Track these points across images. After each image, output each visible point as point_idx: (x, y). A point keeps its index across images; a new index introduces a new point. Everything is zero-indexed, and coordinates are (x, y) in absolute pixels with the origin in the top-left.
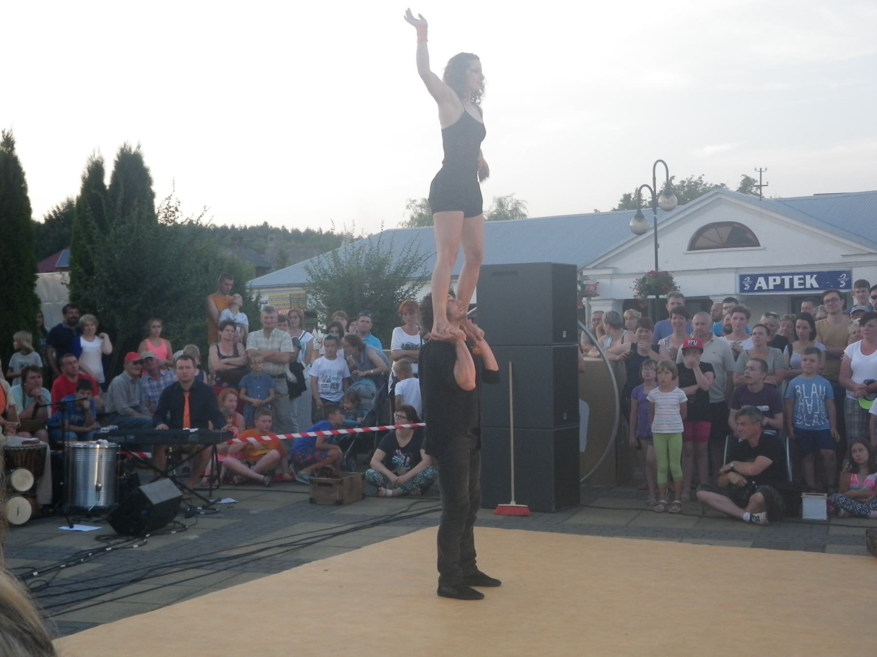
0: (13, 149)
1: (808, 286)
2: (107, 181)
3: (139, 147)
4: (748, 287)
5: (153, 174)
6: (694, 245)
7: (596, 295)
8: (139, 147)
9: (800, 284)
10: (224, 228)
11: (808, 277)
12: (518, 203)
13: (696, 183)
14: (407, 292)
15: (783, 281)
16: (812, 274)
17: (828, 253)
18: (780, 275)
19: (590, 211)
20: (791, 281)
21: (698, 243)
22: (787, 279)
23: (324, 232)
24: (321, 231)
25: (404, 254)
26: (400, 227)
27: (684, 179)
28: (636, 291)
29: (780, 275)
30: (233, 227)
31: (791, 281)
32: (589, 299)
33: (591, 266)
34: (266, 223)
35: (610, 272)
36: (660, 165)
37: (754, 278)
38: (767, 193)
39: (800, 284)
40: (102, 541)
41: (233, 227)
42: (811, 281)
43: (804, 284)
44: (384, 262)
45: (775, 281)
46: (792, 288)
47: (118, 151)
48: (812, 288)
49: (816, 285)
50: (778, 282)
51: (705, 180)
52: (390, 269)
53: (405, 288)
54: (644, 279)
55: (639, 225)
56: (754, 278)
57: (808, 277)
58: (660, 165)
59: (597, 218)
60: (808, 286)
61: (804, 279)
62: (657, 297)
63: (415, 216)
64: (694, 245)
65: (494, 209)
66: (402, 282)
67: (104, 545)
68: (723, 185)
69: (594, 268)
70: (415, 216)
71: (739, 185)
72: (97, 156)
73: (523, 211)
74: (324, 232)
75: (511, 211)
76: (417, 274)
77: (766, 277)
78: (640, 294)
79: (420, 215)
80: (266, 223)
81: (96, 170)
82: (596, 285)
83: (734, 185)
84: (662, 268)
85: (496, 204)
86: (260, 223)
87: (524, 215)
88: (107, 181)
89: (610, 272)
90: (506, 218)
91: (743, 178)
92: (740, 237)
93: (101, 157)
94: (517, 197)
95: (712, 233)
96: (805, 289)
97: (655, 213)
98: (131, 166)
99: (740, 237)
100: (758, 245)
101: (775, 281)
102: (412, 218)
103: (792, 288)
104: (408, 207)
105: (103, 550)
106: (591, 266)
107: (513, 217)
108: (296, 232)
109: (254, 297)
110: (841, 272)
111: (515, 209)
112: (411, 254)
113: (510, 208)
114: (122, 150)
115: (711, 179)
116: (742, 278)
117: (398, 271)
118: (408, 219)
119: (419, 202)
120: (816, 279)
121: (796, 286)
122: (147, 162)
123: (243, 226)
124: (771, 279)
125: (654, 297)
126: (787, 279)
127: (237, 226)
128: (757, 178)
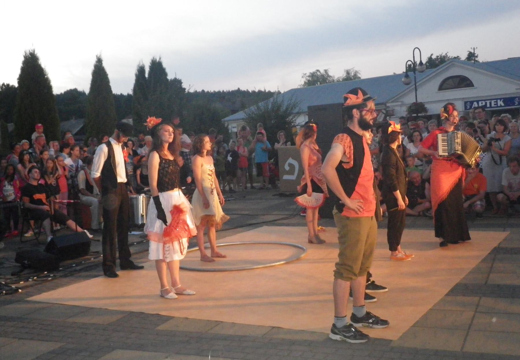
0: (102, 64)
1: (499, 105)
2: (147, 75)
3: (160, 59)
4: (468, 107)
5: (69, 89)
6: (442, 88)
7: (393, 115)
8: (160, 59)
9: (495, 104)
10: (219, 92)
11: (499, 101)
12: (356, 72)
13: (444, 57)
14: (292, 119)
15: (486, 103)
16: (500, 99)
17: (508, 88)
18: (484, 100)
19: (391, 73)
20: (490, 103)
21: (443, 87)
22: (488, 102)
23: (267, 91)
24: (265, 91)
25: (289, 102)
26: (299, 87)
27: (438, 55)
28: (406, 113)
29: (484, 100)
30: (223, 91)
31: (490, 103)
32: (390, 118)
33: (391, 101)
34: (239, 88)
35: (400, 103)
36: (417, 50)
37: (472, 103)
38: (481, 59)
39: (495, 104)
40: (143, 238)
41: (223, 91)
42: (500, 103)
43: (497, 104)
44: (279, 107)
45: (482, 103)
46: (491, 107)
47: (151, 61)
48: (501, 106)
49: (503, 105)
50: (484, 104)
51: (449, 55)
52: (284, 108)
53: (291, 117)
54: (410, 107)
55: (407, 80)
56: (472, 103)
57: (499, 101)
58: (417, 50)
59: (395, 77)
60: (499, 105)
61: (497, 102)
62: (417, 115)
63: (307, 81)
64: (442, 88)
65: (345, 75)
66: (290, 114)
67: (143, 239)
68: (458, 57)
69: (392, 102)
70: (307, 81)
71: (466, 56)
72: (141, 64)
73: (359, 75)
74: (267, 91)
75: (353, 76)
76: (296, 111)
77: (478, 102)
78: (409, 114)
79: (309, 81)
80: (239, 88)
81: (141, 70)
82: (393, 110)
83: (464, 57)
84: (419, 101)
85: (345, 73)
86: (236, 89)
87: (360, 78)
88: (147, 75)
89: (400, 103)
90: (351, 79)
91: (468, 53)
92: (463, 82)
93: (143, 65)
94: (356, 69)
95: (450, 81)
96: (497, 107)
97: (415, 74)
98: (157, 67)
99: (463, 82)
100: (473, 86)
101: (482, 103)
102: (305, 82)
103: (491, 107)
104: (302, 77)
105: (142, 242)
106: (391, 101)
107: (354, 79)
108: (254, 92)
109: (226, 125)
110: (516, 97)
111: (355, 75)
112: (293, 101)
113: (352, 75)
114: (152, 61)
115: (452, 54)
116: (466, 103)
117: (287, 109)
118: (303, 83)
119: (308, 74)
120: (503, 101)
121: (493, 105)
122: (164, 65)
123: (228, 90)
124: (480, 103)
125: (415, 115)
126: (488, 102)
127: (225, 91)
128: (473, 52)
